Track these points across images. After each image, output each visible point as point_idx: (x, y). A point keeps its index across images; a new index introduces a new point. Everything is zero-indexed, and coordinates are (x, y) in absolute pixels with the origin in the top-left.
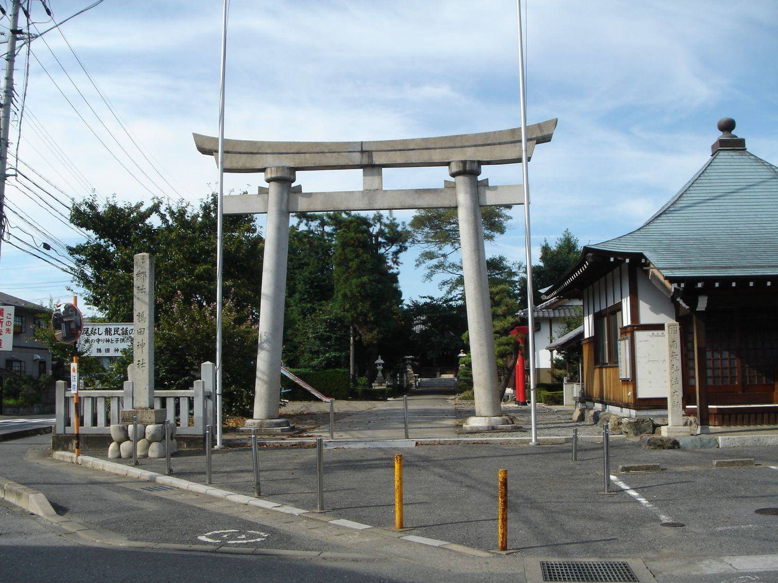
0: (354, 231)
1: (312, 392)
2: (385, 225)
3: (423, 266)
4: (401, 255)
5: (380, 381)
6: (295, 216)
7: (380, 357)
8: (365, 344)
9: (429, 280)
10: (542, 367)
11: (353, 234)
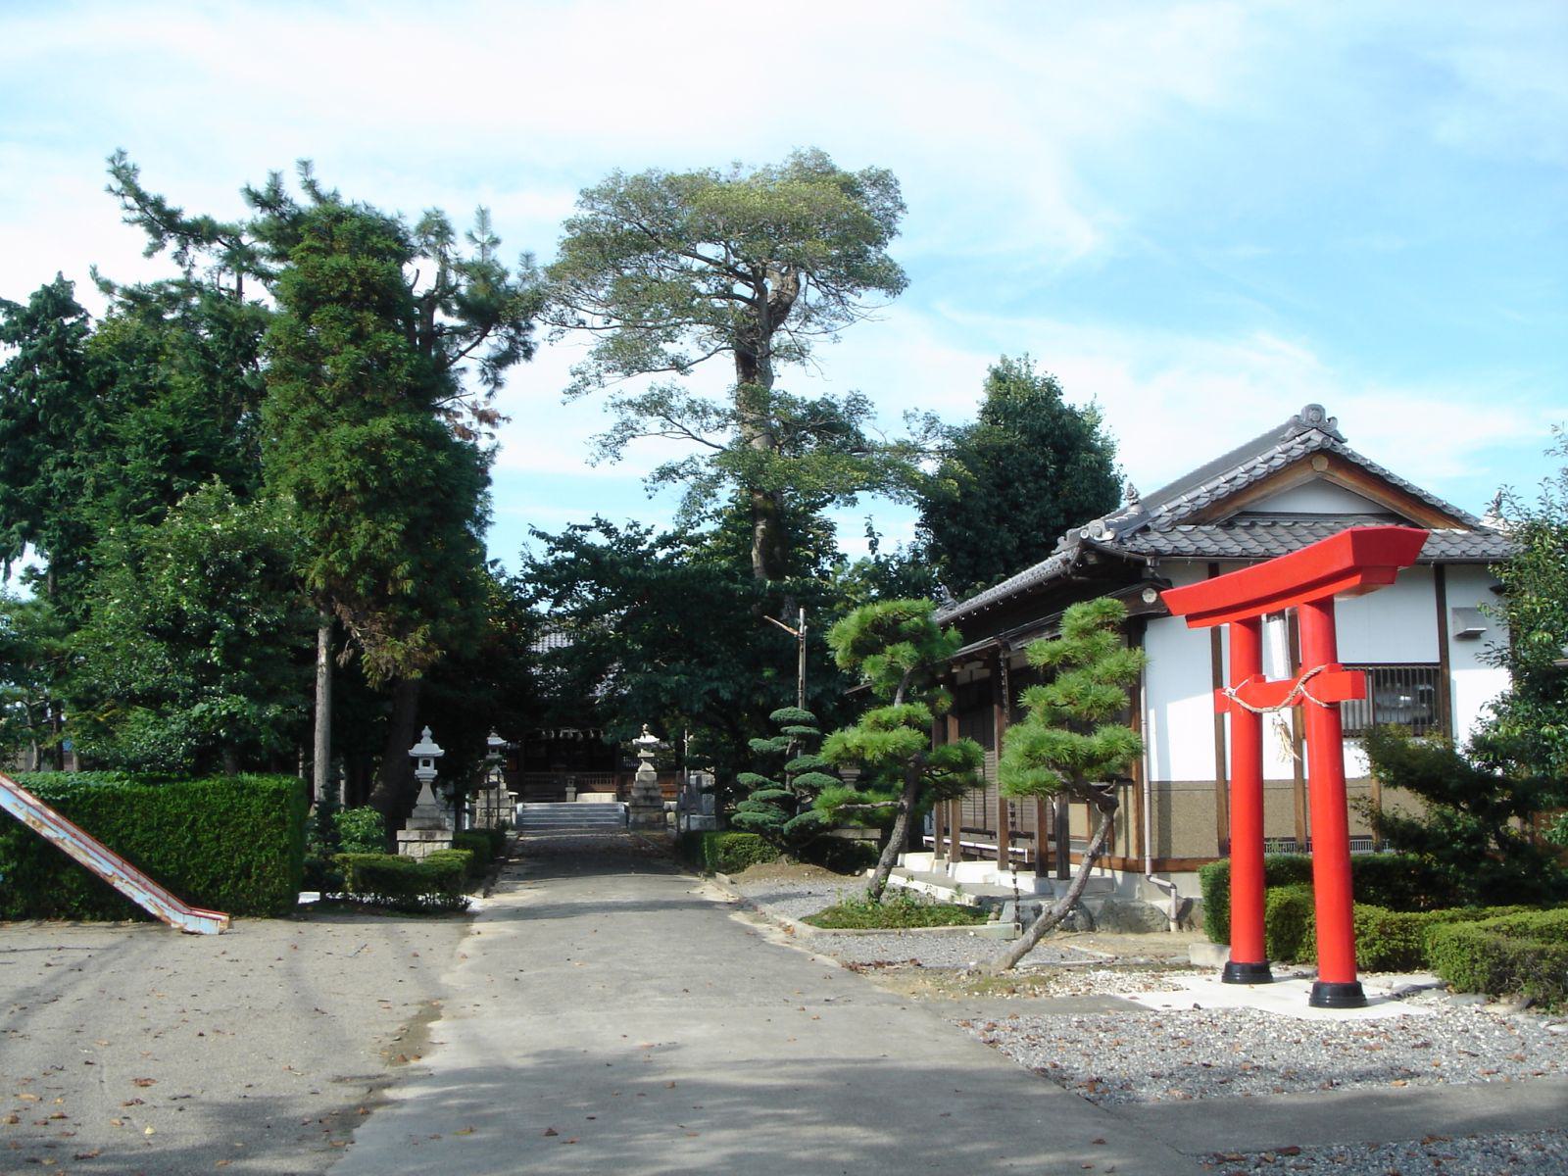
0: (349, 250)
1: (118, 884)
2: (462, 268)
3: (596, 397)
4: (509, 373)
5: (428, 823)
6: (139, 221)
7: (427, 731)
8: (374, 681)
9: (611, 458)
10: (1175, 776)
11: (345, 260)
